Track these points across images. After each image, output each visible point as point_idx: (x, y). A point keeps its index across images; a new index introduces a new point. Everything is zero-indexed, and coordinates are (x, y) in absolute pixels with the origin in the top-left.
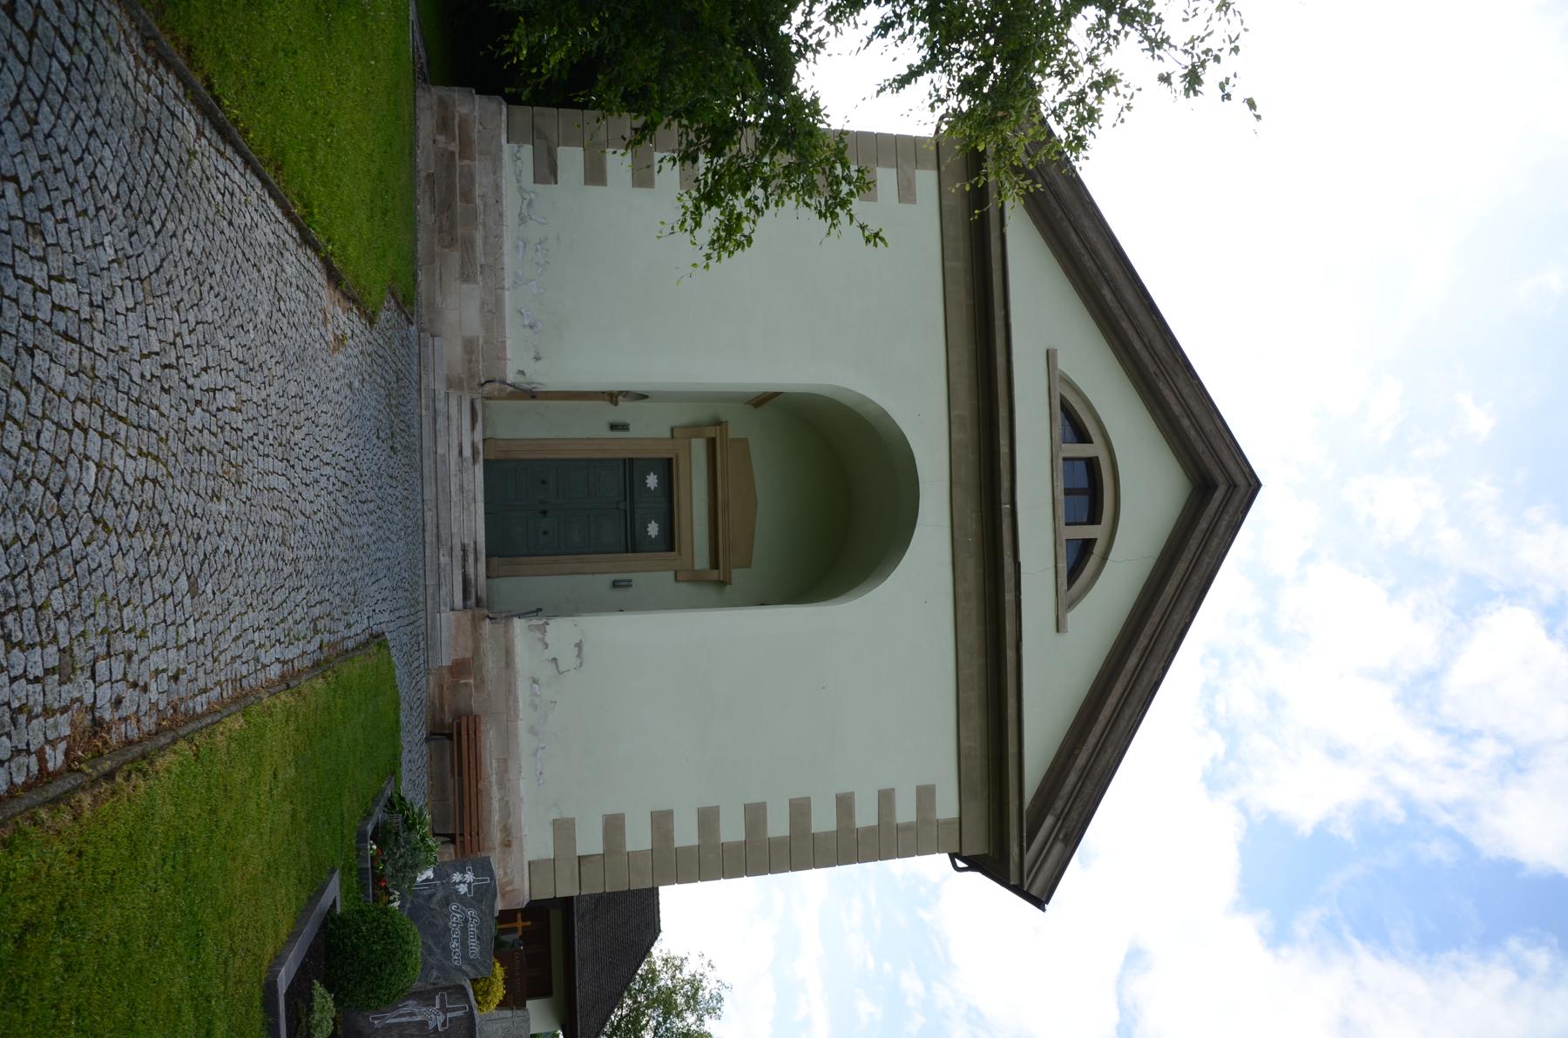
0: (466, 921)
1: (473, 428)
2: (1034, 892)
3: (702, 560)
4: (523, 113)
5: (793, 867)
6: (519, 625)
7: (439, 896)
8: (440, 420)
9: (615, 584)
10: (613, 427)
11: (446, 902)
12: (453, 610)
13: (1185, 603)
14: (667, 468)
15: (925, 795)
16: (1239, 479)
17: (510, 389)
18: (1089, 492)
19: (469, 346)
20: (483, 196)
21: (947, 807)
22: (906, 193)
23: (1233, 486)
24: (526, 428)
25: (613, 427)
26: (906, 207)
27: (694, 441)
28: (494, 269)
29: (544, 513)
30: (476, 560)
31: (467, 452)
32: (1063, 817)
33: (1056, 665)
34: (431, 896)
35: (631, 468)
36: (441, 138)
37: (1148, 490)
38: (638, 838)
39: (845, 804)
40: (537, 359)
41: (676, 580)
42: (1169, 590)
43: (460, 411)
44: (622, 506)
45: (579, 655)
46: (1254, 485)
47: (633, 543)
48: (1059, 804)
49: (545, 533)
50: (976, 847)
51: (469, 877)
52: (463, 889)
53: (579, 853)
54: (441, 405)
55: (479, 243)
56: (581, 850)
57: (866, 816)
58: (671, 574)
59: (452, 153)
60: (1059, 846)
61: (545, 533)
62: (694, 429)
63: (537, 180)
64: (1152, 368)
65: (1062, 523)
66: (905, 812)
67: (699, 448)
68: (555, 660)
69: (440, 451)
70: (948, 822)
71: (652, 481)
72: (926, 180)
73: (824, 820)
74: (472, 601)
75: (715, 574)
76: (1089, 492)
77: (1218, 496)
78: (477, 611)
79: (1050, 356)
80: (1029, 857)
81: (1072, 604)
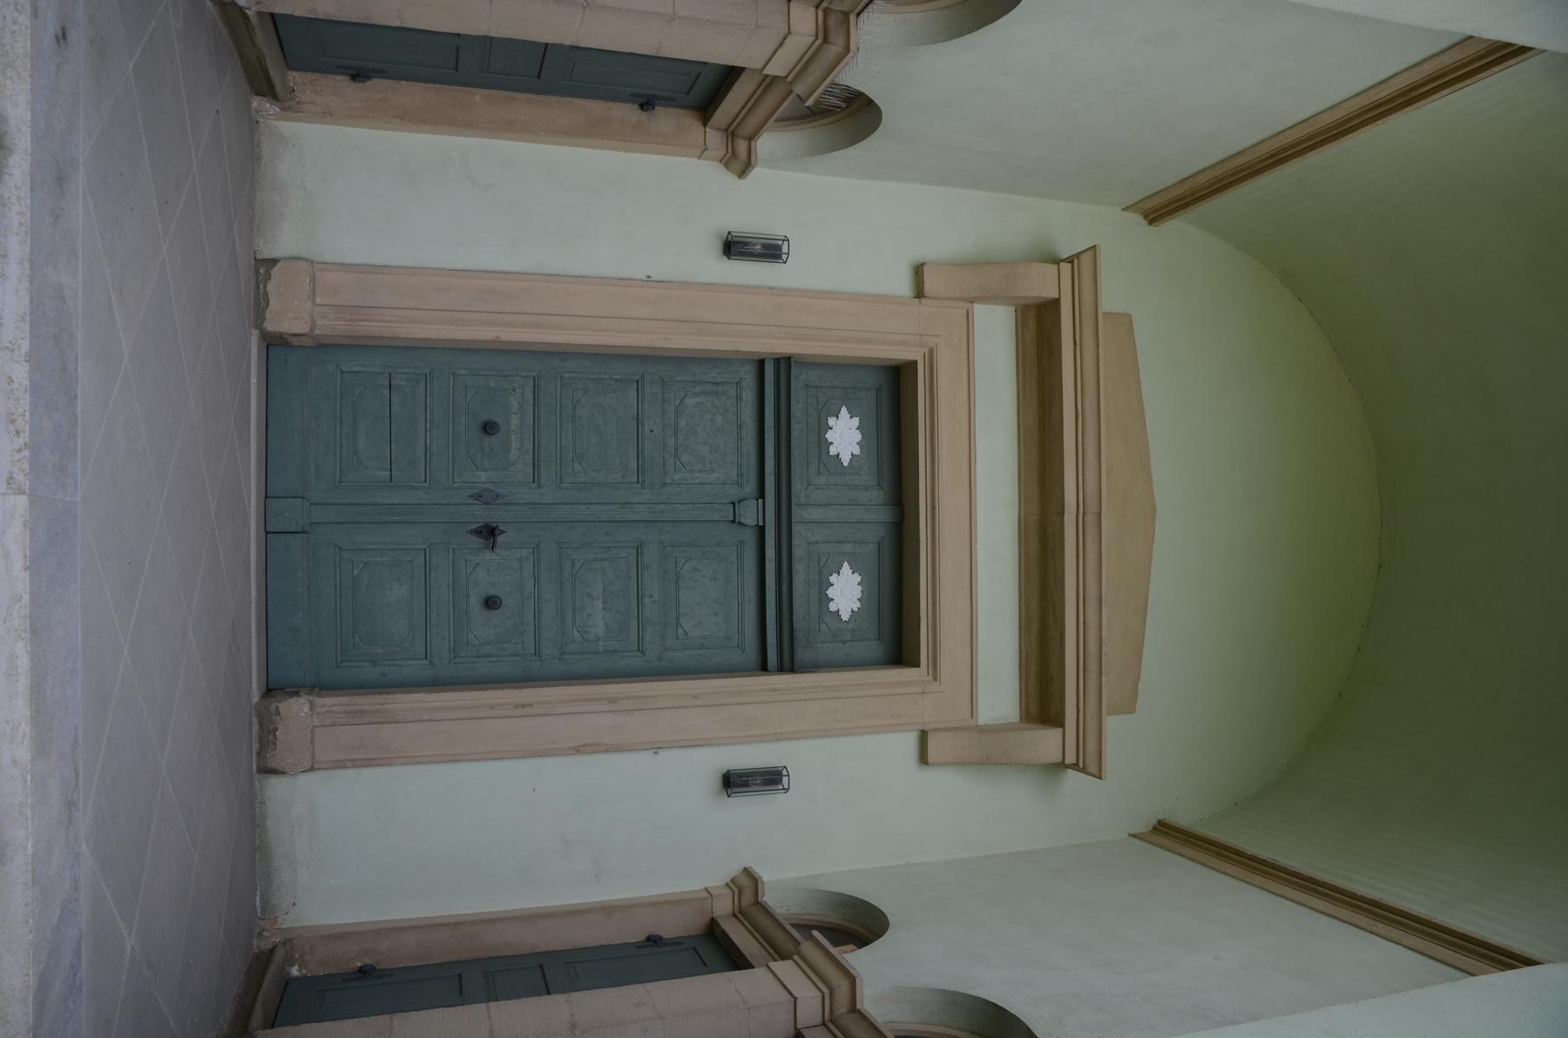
3: (1000, 696)
9: (732, 782)
10: (733, 247)
14: (895, 394)
25: (733, 247)
27: (980, 310)
29: (489, 533)
35: (777, 389)
41: (923, 759)
44: (749, 515)
47: (780, 642)
49: (491, 603)
58: (909, 741)
61: (491, 603)
62: (982, 275)
67: (995, 333)
71: (845, 436)
75: (1047, 743)
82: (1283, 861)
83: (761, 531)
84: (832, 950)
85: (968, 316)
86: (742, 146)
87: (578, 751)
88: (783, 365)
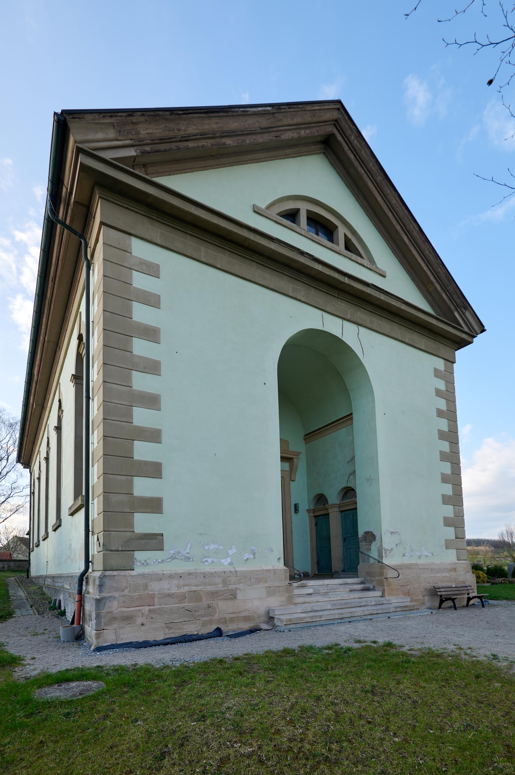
8: (315, 609)
13: (388, 192)
18: (323, 225)
19: (271, 592)
20: (178, 587)
23: (336, 123)
25: (296, 506)
28: (225, 577)
33: (397, 283)
36: (139, 621)
37: (315, 180)
40: (272, 551)
46: (338, 105)
48: (452, 307)
53: (454, 538)
55: (289, 617)
59: (150, 610)
63: (160, 548)
68: (396, 545)
69: (329, 607)
80: (466, 329)
87: (292, 534)
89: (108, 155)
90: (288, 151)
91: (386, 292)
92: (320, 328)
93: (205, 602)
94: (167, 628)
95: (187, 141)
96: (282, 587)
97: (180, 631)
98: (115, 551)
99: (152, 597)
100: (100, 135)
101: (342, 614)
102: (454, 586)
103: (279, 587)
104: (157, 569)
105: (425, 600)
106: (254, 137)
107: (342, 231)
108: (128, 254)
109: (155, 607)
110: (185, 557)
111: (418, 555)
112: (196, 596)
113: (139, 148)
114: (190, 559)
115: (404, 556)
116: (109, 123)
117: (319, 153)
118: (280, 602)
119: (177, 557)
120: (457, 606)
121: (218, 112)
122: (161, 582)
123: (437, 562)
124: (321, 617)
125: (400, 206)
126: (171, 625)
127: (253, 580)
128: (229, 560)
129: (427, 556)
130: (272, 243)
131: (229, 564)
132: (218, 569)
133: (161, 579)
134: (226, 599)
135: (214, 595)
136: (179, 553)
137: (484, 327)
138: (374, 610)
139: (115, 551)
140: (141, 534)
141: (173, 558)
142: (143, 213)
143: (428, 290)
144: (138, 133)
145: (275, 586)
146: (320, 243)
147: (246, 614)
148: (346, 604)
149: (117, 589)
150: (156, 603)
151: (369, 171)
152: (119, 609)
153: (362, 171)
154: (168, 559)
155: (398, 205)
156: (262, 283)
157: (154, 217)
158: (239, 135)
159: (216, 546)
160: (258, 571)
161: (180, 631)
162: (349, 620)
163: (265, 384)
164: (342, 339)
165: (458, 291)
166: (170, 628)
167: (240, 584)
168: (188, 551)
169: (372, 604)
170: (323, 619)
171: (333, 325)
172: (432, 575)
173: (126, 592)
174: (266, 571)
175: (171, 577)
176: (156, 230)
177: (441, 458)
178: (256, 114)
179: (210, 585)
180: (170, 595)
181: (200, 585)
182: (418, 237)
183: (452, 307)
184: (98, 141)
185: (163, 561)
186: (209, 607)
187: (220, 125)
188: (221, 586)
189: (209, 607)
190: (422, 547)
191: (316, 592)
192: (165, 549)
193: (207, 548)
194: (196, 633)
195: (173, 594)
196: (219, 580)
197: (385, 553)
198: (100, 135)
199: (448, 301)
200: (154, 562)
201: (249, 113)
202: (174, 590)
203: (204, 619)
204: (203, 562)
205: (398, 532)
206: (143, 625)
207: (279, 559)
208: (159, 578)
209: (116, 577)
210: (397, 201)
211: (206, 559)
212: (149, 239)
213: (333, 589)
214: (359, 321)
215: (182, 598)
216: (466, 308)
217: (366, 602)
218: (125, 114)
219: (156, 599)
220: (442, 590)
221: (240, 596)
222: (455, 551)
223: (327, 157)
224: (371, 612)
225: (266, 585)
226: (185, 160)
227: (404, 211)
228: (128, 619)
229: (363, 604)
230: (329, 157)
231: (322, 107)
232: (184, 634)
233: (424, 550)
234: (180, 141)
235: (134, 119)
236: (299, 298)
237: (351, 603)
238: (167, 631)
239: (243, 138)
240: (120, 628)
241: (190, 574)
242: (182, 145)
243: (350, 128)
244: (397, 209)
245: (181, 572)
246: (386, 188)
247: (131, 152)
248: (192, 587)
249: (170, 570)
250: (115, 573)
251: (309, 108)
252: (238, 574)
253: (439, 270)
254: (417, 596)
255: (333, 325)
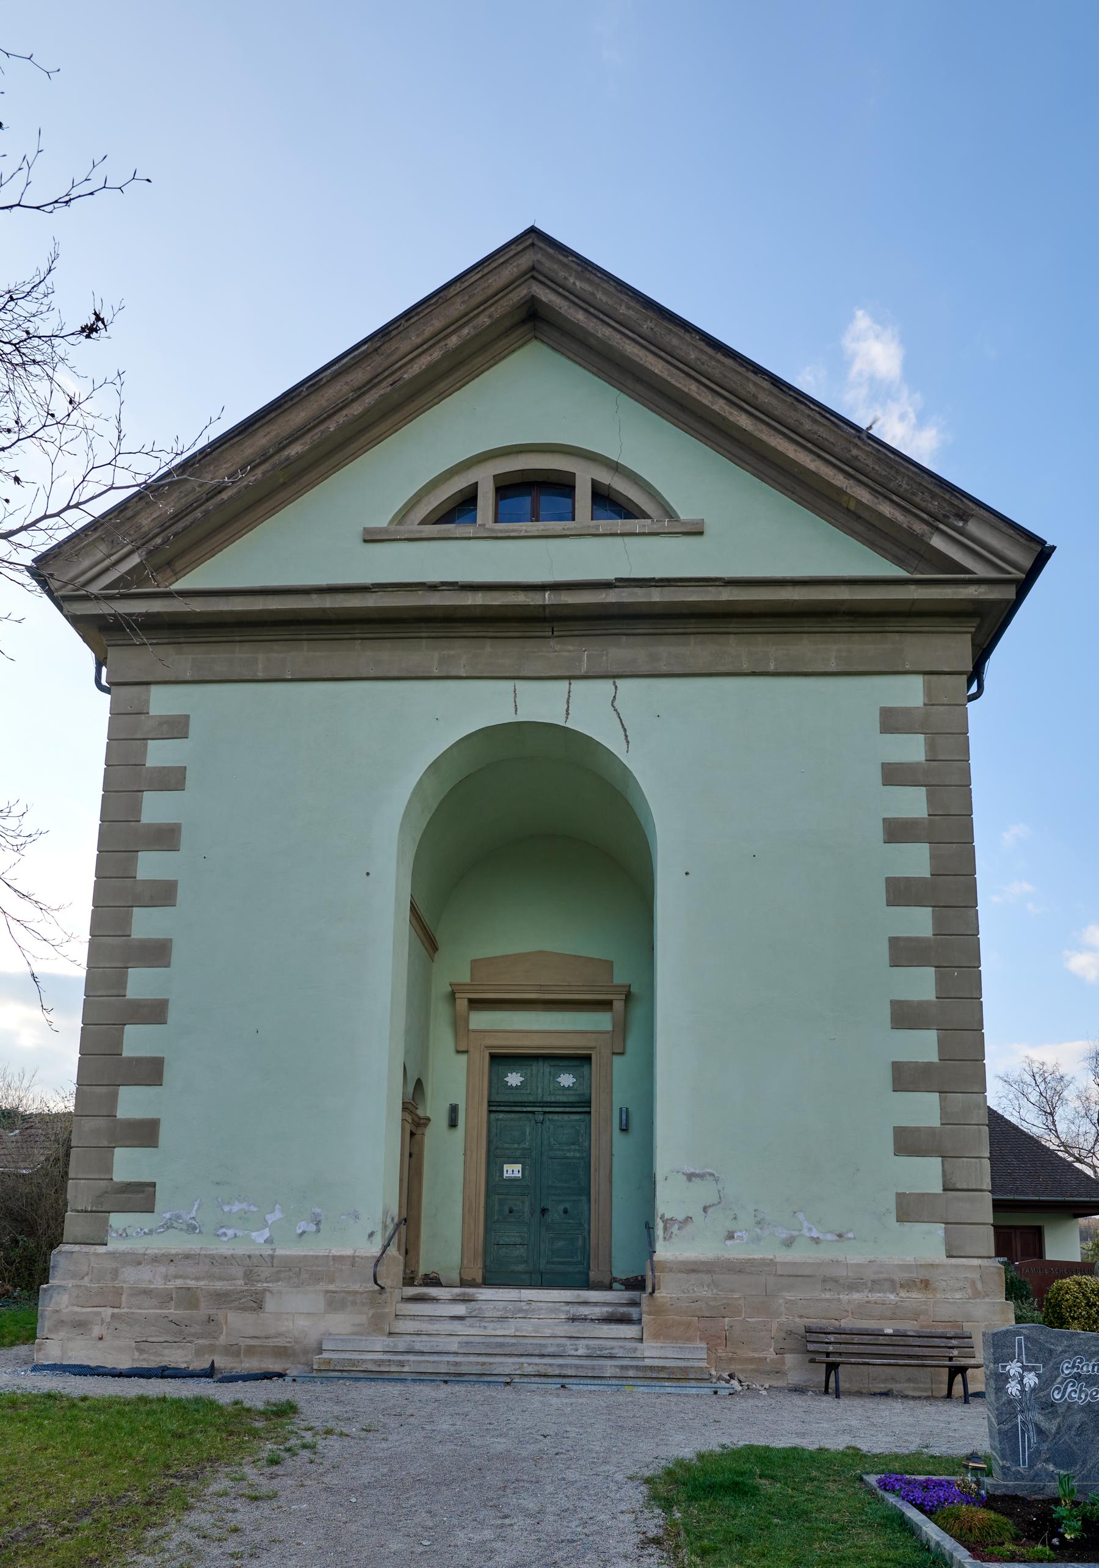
0: (1078, 1377)
1: (434, 1300)
2: (1027, 563)
3: (602, 1021)
4: (73, 1224)
5: (972, 903)
6: (663, 1252)
7: (1038, 1417)
8: (418, 1347)
10: (453, 1124)
11: (1049, 1407)
12: (641, 1340)
13: (675, 342)
14: (501, 1060)
15: (893, 721)
16: (525, 261)
17: (393, 1251)
18: (534, 490)
19: (335, 1303)
20: (166, 1278)
21: (909, 692)
22: (176, 728)
23: (533, 273)
24: (450, 1232)
25: (453, 1124)
26: (193, 728)
27: (472, 1026)
28: (251, 1267)
29: (544, 1211)
30: (585, 1303)
31: (460, 1309)
32: (934, 521)
33: (742, 531)
34: (1040, 1431)
35: (499, 1105)
36: (96, 1331)
37: (534, 404)
38: (924, 1109)
39: (897, 831)
40: (357, 1217)
41: (622, 1054)
42: (657, 367)
43: (414, 1317)
44: (541, 1117)
45: (701, 1176)
47: (582, 1105)
48: (919, 527)
50: (957, 649)
51: (1014, 1368)
52: (1031, 1379)
53: (938, 1189)
54: (401, 1344)
56: (936, 1187)
57: (912, 803)
58: (615, 1058)
59: (113, 1315)
60: (972, 527)
62: (459, 1026)
64: (383, 389)
65: (569, 524)
66: (912, 749)
67: (480, 1020)
68: (705, 1209)
69: (454, 1348)
70: (928, 690)
71: (514, 1079)
72: (163, 701)
73: (915, 861)
74: (634, 1312)
75: (618, 1005)
76: (534, 490)
77: (545, 295)
78: (644, 1307)
79: (372, 538)
80: (981, 571)
81: (669, 513)
82: (614, 1184)
83: (545, 1113)
84: (610, 1309)
85: (474, 1031)
86: (422, 1121)
87: (611, 1182)
88: (494, 1108)
89: (95, 589)
90: (442, 386)
91: (662, 580)
92: (510, 718)
93: (204, 1311)
94: (137, 1349)
95: (220, 492)
96: (361, 1293)
97: (158, 1359)
98: (82, 1211)
99: (119, 1292)
100: (86, 563)
101: (456, 1364)
102: (889, 1331)
103: (356, 1293)
104: (136, 1245)
105: (784, 1363)
106: (344, 412)
107: (584, 477)
108: (143, 717)
109: (123, 1311)
110: (189, 1225)
111: (784, 1236)
112: (189, 1298)
113: (144, 548)
114: (196, 1228)
115: (731, 1236)
116: (94, 540)
117: (529, 340)
118: (354, 1325)
119: (175, 1225)
120: (841, 1389)
121: (263, 417)
122: (140, 1267)
123: (854, 1258)
124: (401, 1364)
125: (711, 357)
126: (143, 1346)
127: (305, 1276)
128: (266, 1233)
129: (816, 1241)
130: (368, 595)
131: (265, 1241)
132: (241, 1250)
133: (140, 1263)
134: (244, 1309)
135: (221, 1298)
136: (178, 1217)
137: (1042, 542)
138: (551, 1365)
139: (82, 1211)
140: (122, 1183)
141: (168, 1226)
142: (166, 641)
143: (848, 510)
144: (140, 527)
145: (346, 1292)
146: (512, 534)
147: (280, 1342)
148: (501, 1345)
149: (74, 1276)
150: (124, 1304)
151: (622, 325)
152: (70, 1308)
153: (608, 331)
154: (160, 1227)
155: (705, 358)
156: (372, 674)
157: (182, 640)
158: (309, 430)
159: (244, 1206)
160: (317, 1257)
161: (158, 1359)
162: (446, 1378)
163: (368, 874)
164: (567, 725)
165: (927, 482)
166: (142, 1351)
167: (278, 1281)
168: (193, 1214)
169: (579, 1353)
170: (406, 1369)
171: (541, 702)
172: (828, 1295)
173: (86, 1282)
174: (334, 1258)
175: (156, 1259)
176: (183, 659)
177: (891, 960)
178: (340, 374)
179: (220, 1279)
180: (146, 1292)
181: (203, 1279)
182: (774, 402)
183: (919, 527)
184: (84, 573)
185: (151, 1232)
186: (210, 1320)
187: (273, 434)
188: (241, 1282)
189: (210, 1320)
190: (801, 1216)
191: (474, 1314)
192: (156, 1209)
193: (226, 1209)
194: (184, 1366)
195: (151, 1291)
196: (238, 1271)
197: (665, 1229)
198: (86, 563)
199: (899, 517)
200: (138, 1233)
201: (324, 380)
202: (159, 1284)
203: (201, 1341)
204: (218, 1235)
205: (712, 1175)
206: (101, 1339)
207: (371, 1235)
208: (137, 1260)
209: (75, 1255)
210: (702, 351)
211: (224, 1230)
212: (172, 679)
213: (521, 1310)
214: (614, 670)
215: (166, 1298)
216: (964, 516)
217: (558, 1345)
218: (116, 513)
219: (124, 1298)
220: (832, 1338)
221: (270, 1304)
222: (939, 1229)
223: (543, 341)
224: (542, 1370)
225: (332, 1287)
226: (236, 517)
227: (722, 363)
228: (81, 1325)
229: (550, 1350)
230: (545, 339)
231: (486, 271)
232: (163, 1364)
233: (805, 1224)
234: (207, 500)
235: (129, 513)
236: (453, 674)
237: (513, 1345)
238: (137, 1354)
239: (322, 428)
240: (69, 1339)
241: (187, 1257)
242: (210, 505)
243: (564, 265)
244: (704, 368)
245: (173, 1251)
246: (668, 338)
247: (135, 560)
248: (189, 1281)
249: (159, 1249)
250: (77, 1248)
251: (452, 291)
252: (275, 1261)
253: (855, 452)
254: (754, 1350)
255: (541, 702)
